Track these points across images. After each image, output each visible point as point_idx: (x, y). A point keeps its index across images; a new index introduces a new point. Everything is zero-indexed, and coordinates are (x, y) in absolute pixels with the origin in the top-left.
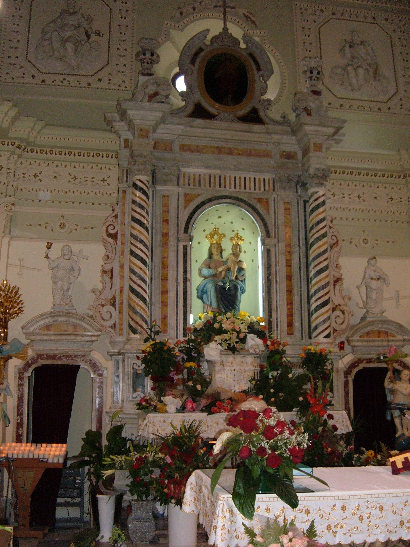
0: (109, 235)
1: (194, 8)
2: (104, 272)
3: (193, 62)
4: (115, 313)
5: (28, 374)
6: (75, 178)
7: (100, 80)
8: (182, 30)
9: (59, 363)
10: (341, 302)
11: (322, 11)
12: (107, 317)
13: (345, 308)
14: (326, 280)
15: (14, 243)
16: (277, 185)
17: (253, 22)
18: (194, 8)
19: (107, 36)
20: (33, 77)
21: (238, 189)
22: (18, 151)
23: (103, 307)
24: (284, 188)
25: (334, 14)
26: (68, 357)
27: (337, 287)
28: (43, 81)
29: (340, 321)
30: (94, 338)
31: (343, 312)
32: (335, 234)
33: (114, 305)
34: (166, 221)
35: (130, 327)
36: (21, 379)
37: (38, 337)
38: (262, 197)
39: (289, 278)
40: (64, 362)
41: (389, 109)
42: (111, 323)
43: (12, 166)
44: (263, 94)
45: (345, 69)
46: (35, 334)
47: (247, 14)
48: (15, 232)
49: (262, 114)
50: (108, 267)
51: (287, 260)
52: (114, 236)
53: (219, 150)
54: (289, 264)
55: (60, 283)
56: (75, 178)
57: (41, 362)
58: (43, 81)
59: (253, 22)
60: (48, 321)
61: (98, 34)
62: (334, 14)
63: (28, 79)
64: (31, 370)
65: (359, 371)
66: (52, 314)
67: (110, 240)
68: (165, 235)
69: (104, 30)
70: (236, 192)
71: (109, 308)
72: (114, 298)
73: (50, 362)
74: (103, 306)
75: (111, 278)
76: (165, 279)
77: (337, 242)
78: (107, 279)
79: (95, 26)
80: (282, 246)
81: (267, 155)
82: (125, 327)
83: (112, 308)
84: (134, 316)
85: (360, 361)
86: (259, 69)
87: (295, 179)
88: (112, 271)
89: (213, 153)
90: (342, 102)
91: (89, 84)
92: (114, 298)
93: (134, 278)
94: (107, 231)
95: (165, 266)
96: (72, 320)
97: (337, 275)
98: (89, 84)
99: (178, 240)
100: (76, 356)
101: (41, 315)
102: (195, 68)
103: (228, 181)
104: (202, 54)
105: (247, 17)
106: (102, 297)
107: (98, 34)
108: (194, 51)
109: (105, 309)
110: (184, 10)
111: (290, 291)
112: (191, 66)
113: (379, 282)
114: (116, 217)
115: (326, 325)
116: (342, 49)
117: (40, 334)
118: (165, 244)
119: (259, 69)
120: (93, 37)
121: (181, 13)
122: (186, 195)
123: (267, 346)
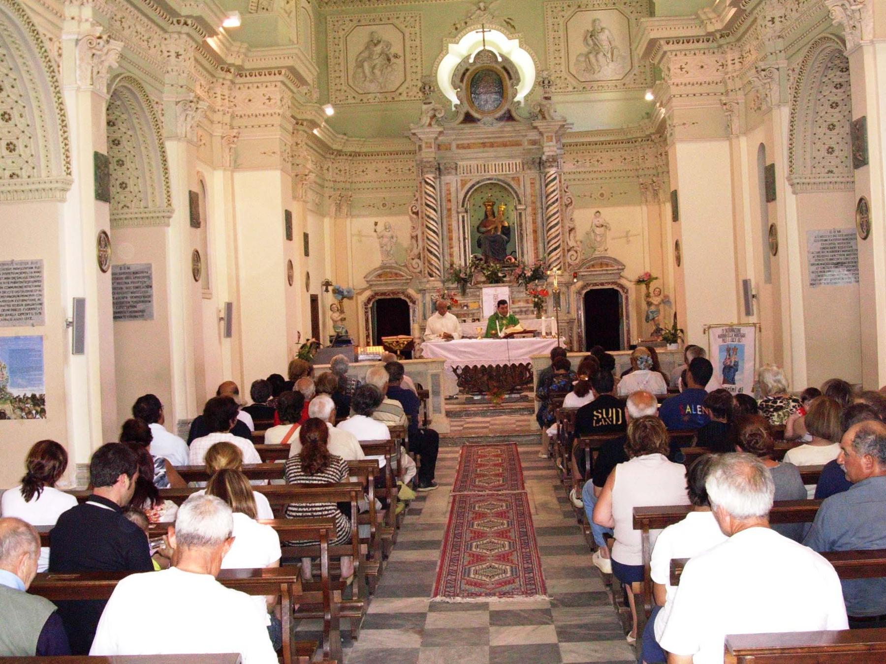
0: (414, 213)
1: (466, 23)
2: (412, 237)
3: (462, 81)
4: (421, 264)
5: (370, 305)
6: (390, 170)
7: (400, 94)
8: (458, 43)
9: (388, 297)
10: (575, 244)
11: (569, 6)
12: (416, 266)
13: (578, 249)
14: (557, 232)
15: (354, 220)
16: (526, 167)
17: (513, 27)
18: (466, 23)
19: (402, 58)
20: (354, 97)
21: (497, 173)
22: (351, 158)
23: (179, 505)
24: (530, 169)
25: (579, 7)
26: (394, 293)
27: (572, 235)
28: (362, 100)
29: (573, 258)
30: (409, 281)
31: (576, 252)
32: (571, 196)
33: (419, 258)
34: (450, 201)
35: (429, 273)
36: (366, 308)
37: (374, 283)
38: (515, 176)
39: (535, 232)
40: (392, 296)
41: (624, 84)
42: (418, 270)
43: (347, 168)
44: (514, 98)
45: (587, 55)
46: (372, 281)
47: (508, 20)
48: (355, 212)
49: (514, 114)
50: (414, 234)
51: (533, 219)
52: (417, 213)
53: (484, 145)
54: (534, 222)
55: (385, 247)
56: (390, 170)
57: (378, 297)
58: (362, 100)
59: (513, 27)
60: (380, 272)
61: (396, 56)
62: (579, 7)
63: (351, 101)
64: (371, 303)
65: (407, 303)
66: (381, 268)
67: (414, 216)
68: (449, 210)
69: (400, 53)
70: (496, 175)
71: (417, 260)
72: (419, 254)
73: (383, 297)
74: (413, 259)
75: (417, 241)
76: (451, 239)
77: (571, 202)
78: (414, 242)
79: (393, 50)
80: (529, 210)
81: (518, 144)
82: (427, 274)
83: (418, 261)
84: (430, 266)
85: (588, 285)
86: (510, 78)
87: (538, 161)
88: (417, 236)
89: (479, 147)
90: (585, 85)
91: (393, 98)
92: (419, 254)
93: (429, 242)
94: (412, 210)
95: (450, 231)
96: (394, 271)
97: (572, 226)
98: (393, 98)
99: (458, 213)
100: (398, 293)
101: (375, 269)
102: (464, 85)
103: (490, 167)
104: (468, 74)
105: (508, 23)
106: (412, 253)
107: (396, 56)
108: (462, 71)
109: (414, 262)
110: (458, 26)
111: (536, 241)
112: (461, 84)
113: (603, 229)
114: (417, 200)
115: (558, 262)
116: (585, 39)
117: (375, 281)
118: (449, 216)
119: (510, 78)
120: (393, 60)
121: (456, 29)
122: (462, 180)
123: (510, 282)
